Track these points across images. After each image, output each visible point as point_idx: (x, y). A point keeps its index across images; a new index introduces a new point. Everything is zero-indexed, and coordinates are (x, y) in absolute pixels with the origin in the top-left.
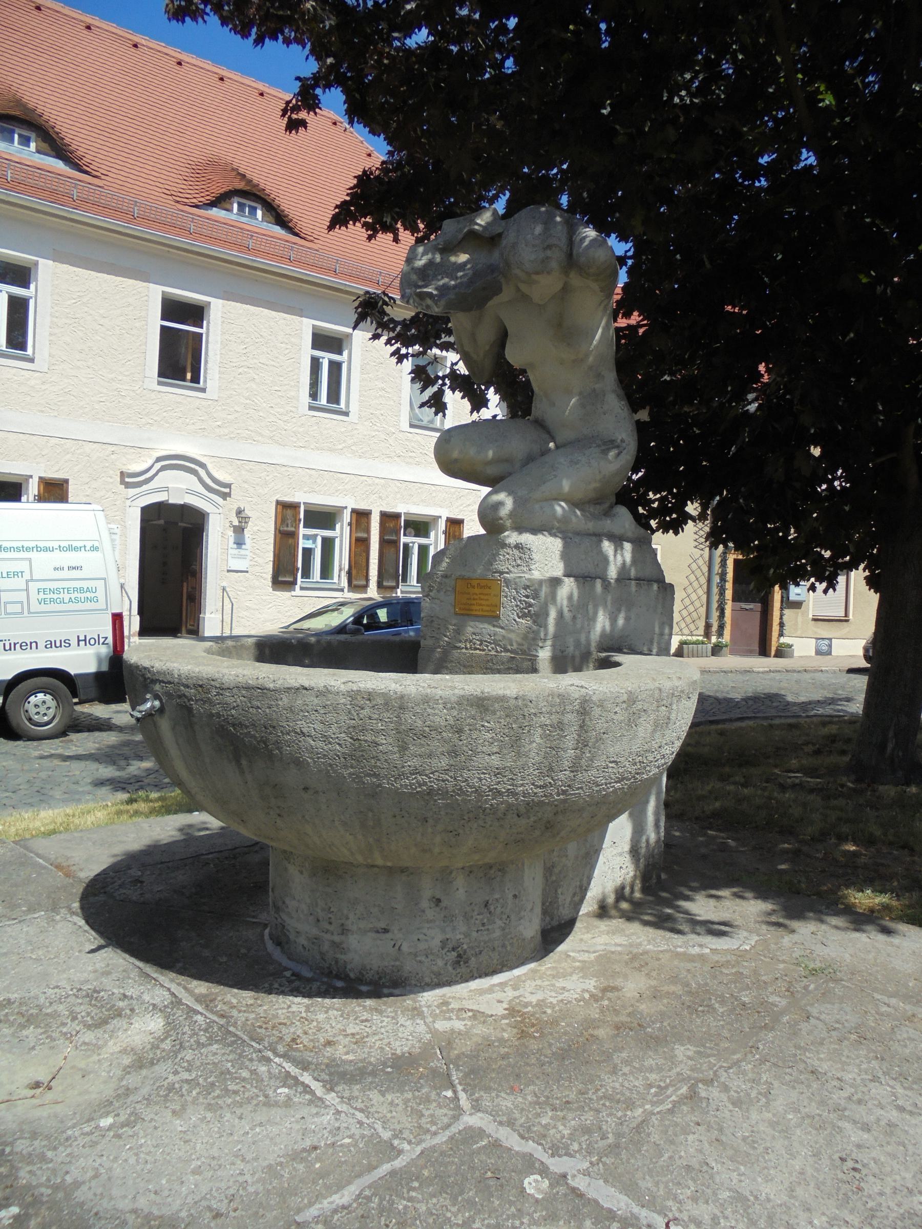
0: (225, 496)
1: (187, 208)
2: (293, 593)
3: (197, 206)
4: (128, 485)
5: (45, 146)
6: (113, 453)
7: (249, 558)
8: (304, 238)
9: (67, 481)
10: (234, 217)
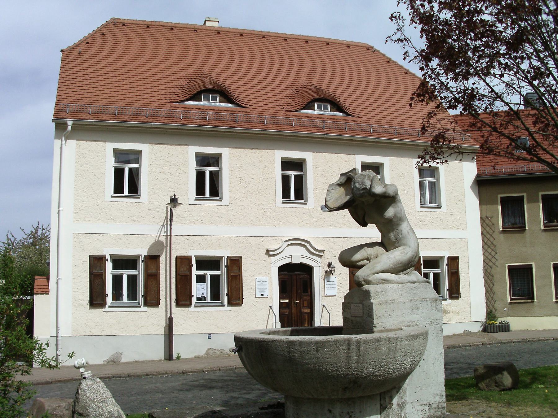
0: (321, 256)
1: (292, 113)
2: (104, 310)
3: (296, 111)
4: (271, 256)
5: (222, 98)
6: (263, 241)
7: (336, 289)
8: (354, 116)
9: (241, 257)
10: (316, 112)
